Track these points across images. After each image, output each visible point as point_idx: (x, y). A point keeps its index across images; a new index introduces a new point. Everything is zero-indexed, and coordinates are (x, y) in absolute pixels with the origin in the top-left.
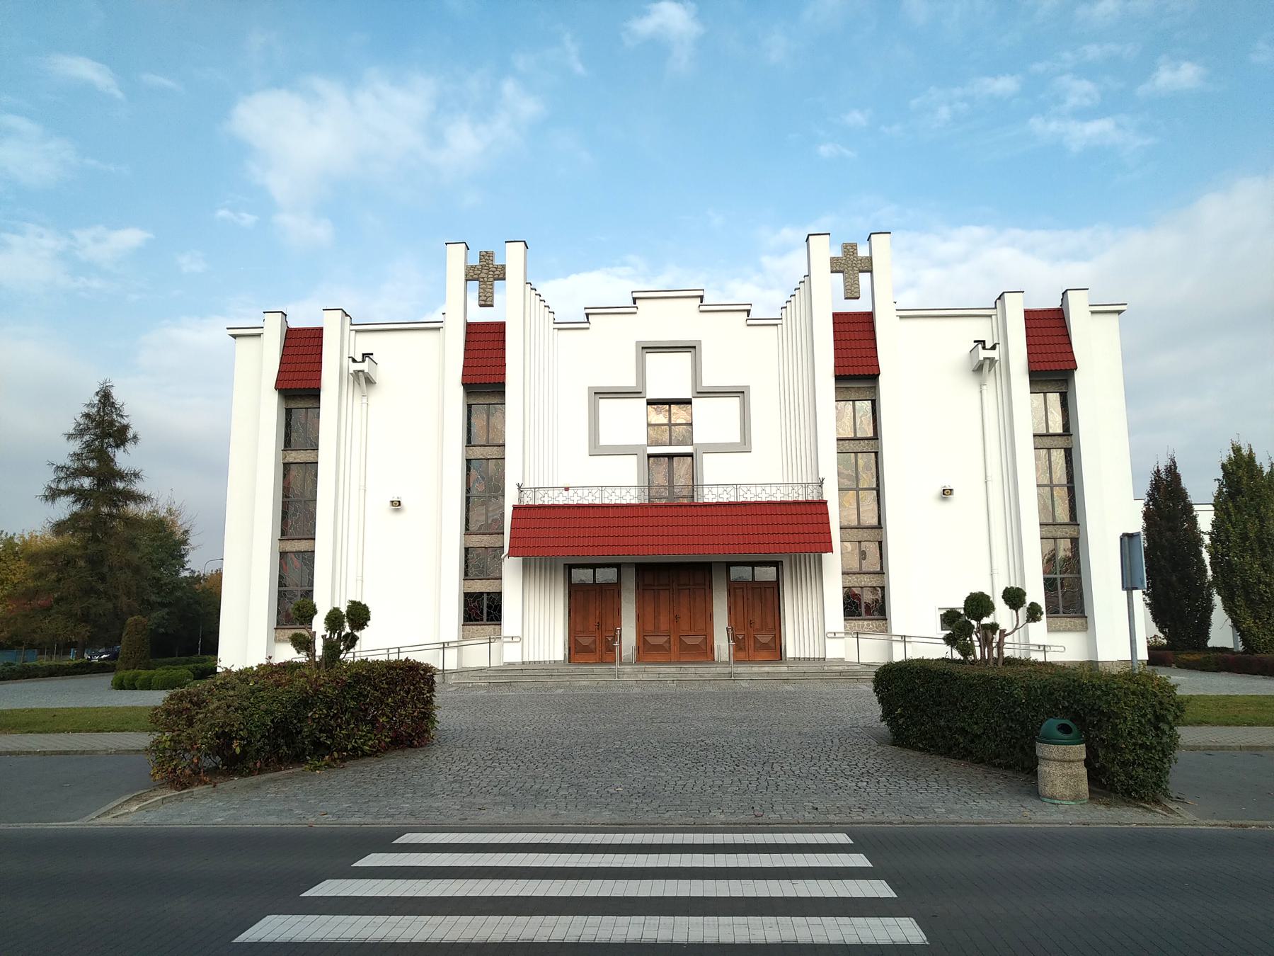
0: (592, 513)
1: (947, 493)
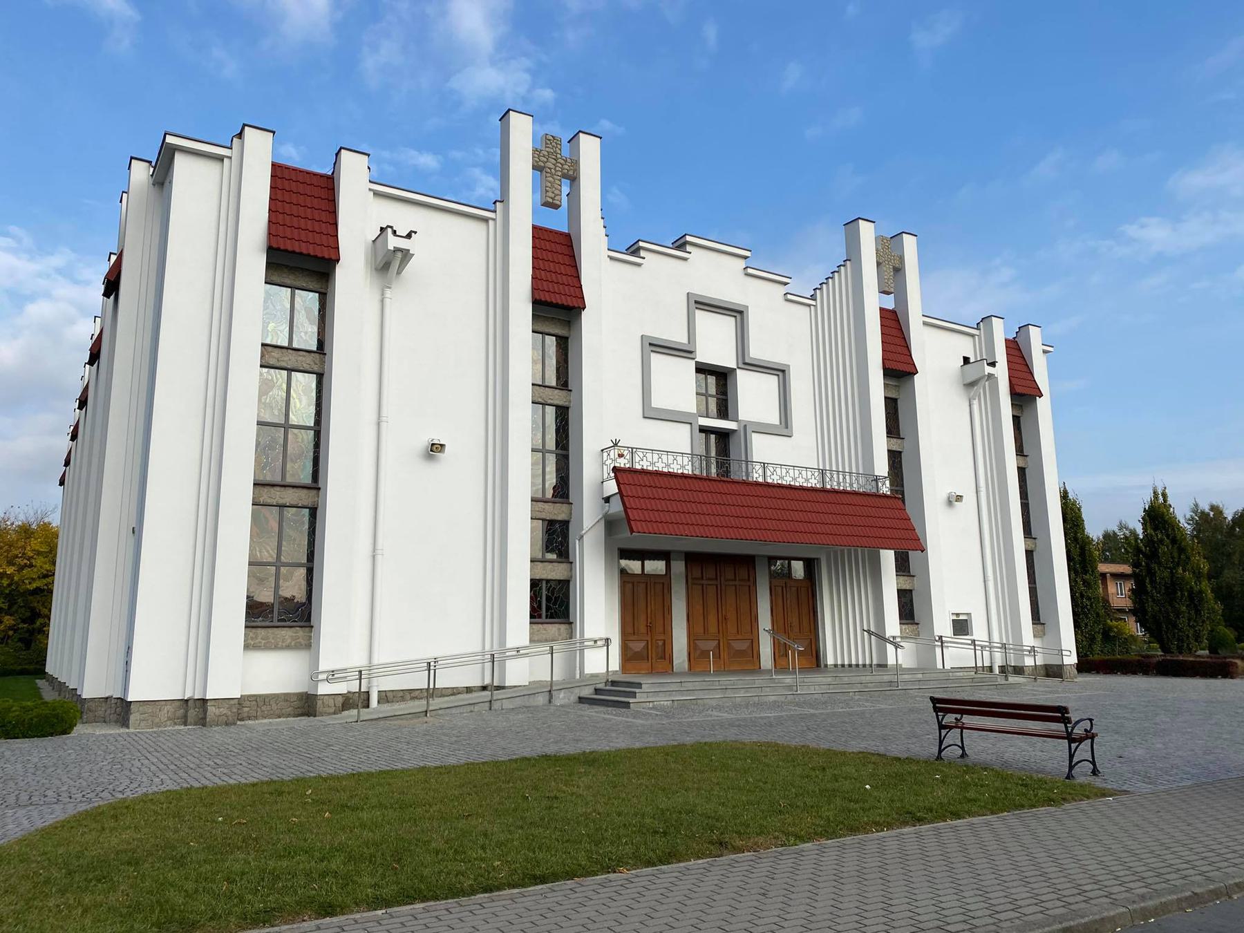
0: (845, 499)
1: (436, 448)
